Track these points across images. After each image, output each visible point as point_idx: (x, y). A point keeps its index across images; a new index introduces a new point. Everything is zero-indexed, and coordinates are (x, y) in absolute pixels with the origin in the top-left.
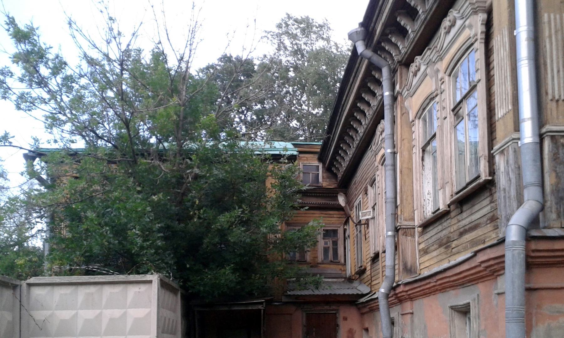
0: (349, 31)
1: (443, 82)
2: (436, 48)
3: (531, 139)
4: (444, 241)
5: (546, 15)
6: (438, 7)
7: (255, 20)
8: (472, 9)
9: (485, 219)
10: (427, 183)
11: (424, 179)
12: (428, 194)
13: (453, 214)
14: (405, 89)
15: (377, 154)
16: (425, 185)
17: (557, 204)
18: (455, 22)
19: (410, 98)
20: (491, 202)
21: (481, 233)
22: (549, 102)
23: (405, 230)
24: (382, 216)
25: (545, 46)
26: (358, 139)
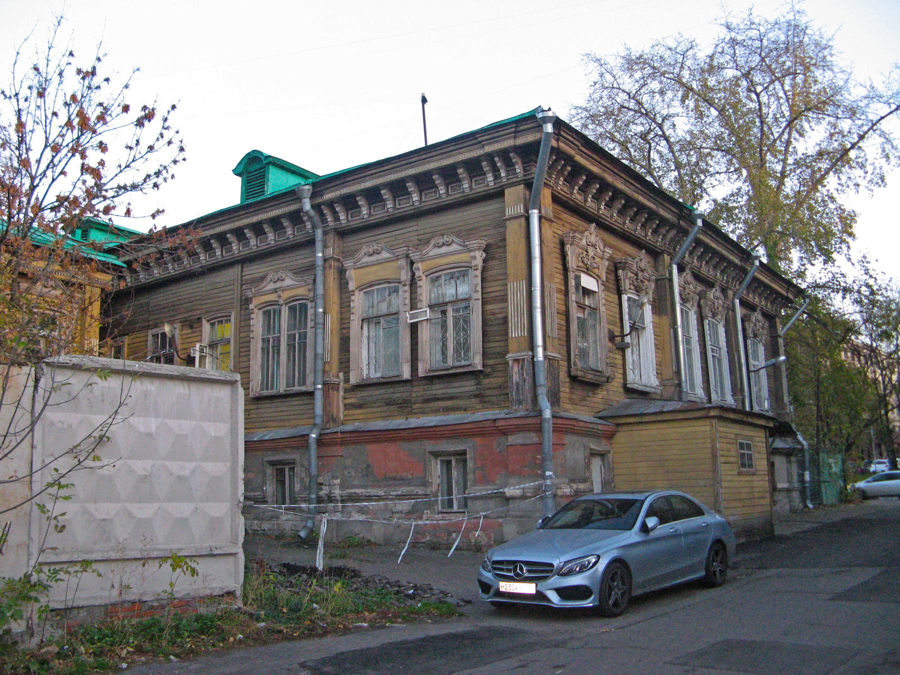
4: (400, 401)
13: (414, 383)
18: (451, 244)
20: (477, 384)
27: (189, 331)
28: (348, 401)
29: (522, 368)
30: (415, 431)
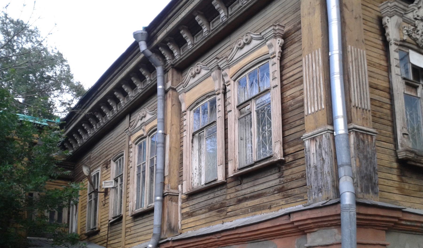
0: (135, 31)
1: (230, 84)
2: (227, 58)
3: (344, 131)
4: (218, 206)
5: (349, 46)
6: (224, 29)
7: (35, 2)
8: (274, 33)
9: (272, 190)
10: (195, 160)
11: (193, 157)
12: (195, 169)
13: (229, 185)
14: (181, 86)
15: (131, 135)
16: (194, 162)
17: (360, 181)
18: (251, 41)
19: (184, 93)
20: (280, 177)
21: (265, 201)
22: (353, 107)
23: (171, 196)
24: (133, 186)
25: (349, 68)
26: (103, 122)
27: (106, 171)
28: (184, 211)
29: (320, 146)
30: (223, 234)
